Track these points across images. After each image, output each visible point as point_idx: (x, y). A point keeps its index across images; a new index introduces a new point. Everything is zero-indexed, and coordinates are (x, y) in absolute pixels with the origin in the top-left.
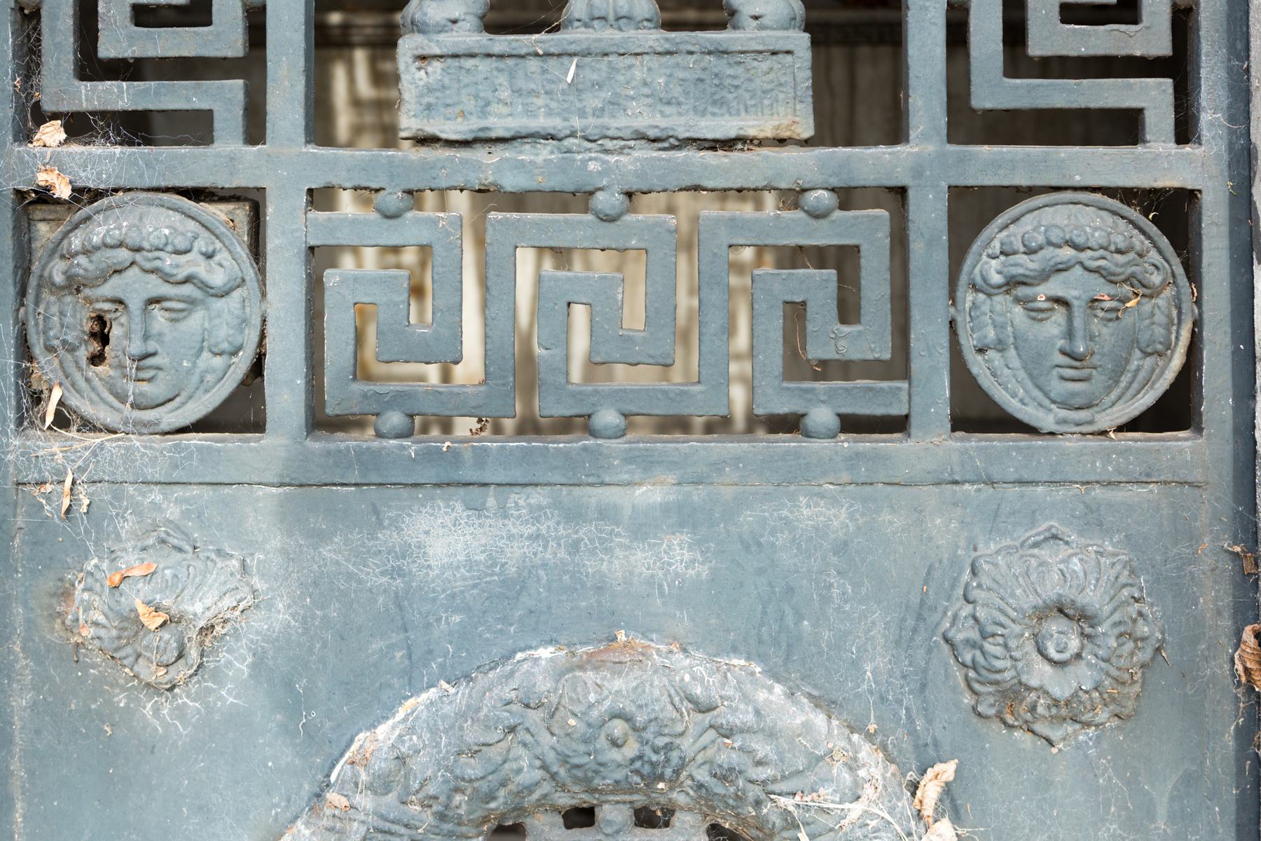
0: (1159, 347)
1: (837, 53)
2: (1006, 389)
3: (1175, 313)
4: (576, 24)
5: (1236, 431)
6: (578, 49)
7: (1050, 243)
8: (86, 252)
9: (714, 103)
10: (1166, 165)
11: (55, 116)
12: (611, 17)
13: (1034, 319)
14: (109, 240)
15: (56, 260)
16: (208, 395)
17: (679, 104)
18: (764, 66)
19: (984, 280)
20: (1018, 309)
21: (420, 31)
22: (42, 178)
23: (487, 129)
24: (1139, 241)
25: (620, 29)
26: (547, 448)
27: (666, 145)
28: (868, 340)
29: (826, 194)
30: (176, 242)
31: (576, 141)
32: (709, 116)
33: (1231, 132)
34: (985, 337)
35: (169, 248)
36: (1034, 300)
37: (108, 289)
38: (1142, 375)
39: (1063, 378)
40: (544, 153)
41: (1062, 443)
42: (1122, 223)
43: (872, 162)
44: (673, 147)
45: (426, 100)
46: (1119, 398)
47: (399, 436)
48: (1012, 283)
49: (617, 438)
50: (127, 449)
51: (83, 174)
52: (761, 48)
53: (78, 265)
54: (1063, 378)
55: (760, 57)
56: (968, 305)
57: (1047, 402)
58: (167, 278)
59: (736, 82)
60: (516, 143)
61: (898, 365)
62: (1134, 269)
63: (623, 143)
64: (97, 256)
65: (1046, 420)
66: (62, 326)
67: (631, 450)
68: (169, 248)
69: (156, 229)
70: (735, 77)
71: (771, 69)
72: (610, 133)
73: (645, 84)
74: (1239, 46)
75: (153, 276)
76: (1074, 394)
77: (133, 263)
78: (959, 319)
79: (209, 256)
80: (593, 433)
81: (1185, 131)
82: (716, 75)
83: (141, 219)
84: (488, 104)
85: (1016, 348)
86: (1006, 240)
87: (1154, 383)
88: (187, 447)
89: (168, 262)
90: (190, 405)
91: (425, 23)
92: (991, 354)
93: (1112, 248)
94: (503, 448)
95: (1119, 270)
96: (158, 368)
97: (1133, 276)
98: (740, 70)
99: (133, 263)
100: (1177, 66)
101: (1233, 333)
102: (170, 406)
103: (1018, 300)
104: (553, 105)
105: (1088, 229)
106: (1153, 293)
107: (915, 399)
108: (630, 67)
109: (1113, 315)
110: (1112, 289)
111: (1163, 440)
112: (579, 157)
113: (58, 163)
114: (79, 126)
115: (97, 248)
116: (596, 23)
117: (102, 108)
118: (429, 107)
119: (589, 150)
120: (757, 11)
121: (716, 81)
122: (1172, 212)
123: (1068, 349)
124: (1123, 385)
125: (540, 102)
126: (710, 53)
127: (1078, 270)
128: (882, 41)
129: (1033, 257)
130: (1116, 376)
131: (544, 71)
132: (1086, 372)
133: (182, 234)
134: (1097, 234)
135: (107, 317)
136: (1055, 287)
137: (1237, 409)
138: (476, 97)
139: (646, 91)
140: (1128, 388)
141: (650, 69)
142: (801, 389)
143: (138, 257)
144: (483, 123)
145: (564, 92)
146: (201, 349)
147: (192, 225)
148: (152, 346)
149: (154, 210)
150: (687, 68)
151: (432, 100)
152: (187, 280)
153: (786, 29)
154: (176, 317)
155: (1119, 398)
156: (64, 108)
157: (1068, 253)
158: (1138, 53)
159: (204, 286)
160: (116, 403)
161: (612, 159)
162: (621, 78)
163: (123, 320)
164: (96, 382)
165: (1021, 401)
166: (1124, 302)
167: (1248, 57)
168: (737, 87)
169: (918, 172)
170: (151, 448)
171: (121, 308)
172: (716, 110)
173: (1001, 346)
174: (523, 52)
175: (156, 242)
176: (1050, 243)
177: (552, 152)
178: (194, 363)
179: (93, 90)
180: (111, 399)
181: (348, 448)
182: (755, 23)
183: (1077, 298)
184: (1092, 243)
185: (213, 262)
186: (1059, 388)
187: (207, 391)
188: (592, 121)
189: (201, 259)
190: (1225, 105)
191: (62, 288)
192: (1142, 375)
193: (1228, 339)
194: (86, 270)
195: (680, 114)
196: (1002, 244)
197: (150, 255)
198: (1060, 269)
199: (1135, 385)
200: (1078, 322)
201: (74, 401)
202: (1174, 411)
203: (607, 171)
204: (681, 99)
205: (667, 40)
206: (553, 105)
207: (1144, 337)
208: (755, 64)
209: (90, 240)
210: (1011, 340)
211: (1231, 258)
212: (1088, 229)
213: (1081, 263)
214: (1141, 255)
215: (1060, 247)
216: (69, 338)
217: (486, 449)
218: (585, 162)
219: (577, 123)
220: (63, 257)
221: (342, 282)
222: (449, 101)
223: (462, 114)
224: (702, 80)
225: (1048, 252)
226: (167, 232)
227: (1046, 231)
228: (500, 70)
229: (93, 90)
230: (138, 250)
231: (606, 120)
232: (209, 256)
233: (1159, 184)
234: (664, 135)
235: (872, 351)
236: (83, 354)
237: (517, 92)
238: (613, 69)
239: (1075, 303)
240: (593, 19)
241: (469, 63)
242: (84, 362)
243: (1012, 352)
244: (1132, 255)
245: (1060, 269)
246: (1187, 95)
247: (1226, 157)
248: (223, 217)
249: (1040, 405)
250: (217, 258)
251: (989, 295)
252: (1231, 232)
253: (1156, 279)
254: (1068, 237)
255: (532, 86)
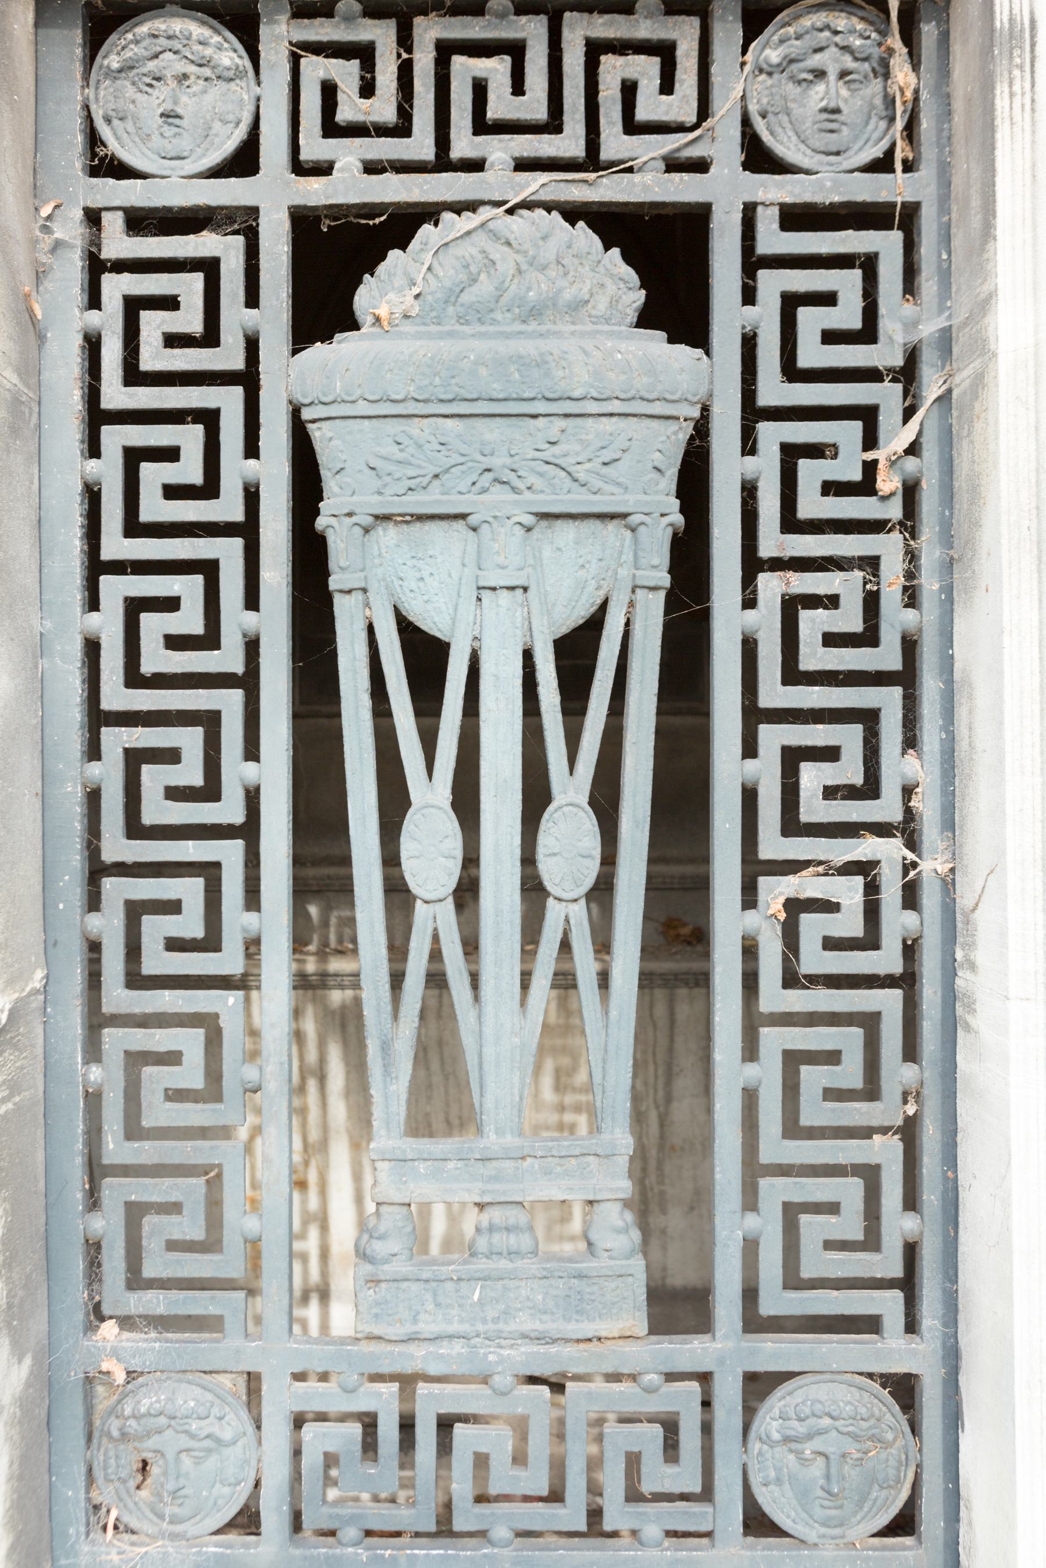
0: (892, 1483)
1: (660, 994)
2: (783, 1512)
3: (903, 1457)
4: (480, 1256)
5: (946, 1545)
6: (482, 1276)
7: (814, 1415)
8: (134, 1417)
9: (577, 1312)
10: (897, 1357)
11: (111, 1318)
12: (505, 1252)
13: (803, 1465)
14: (152, 1412)
15: (113, 1418)
16: (220, 1514)
17: (553, 1313)
18: (613, 1285)
19: (768, 1437)
20: (792, 1457)
21: (370, 1262)
22: (105, 1366)
23: (418, 1333)
24: (878, 1409)
25: (511, 1261)
26: (459, 1555)
27: (543, 1342)
28: (686, 1476)
29: (655, 1376)
30: (200, 1411)
31: (480, 1340)
32: (573, 1322)
33: (945, 1334)
34: (768, 1476)
35: (195, 1416)
36: (803, 1453)
37: (151, 1443)
38: (879, 1502)
39: (822, 1506)
40: (458, 1348)
41: (822, 1552)
42: (866, 1395)
43: (691, 1351)
44: (548, 1343)
45: (375, 1311)
46: (863, 1518)
47: (354, 1545)
48: (787, 1440)
49: (507, 1546)
50: (164, 1553)
51: (133, 1362)
52: (610, 1273)
53: (130, 1426)
54: (822, 1506)
55: (610, 1279)
56: (756, 1452)
57: (811, 1522)
58: (192, 1436)
59: (593, 1297)
60: (438, 1341)
61: (707, 1494)
62: (873, 1431)
63: (513, 1342)
64: (143, 1421)
65: (811, 1536)
66: (118, 1467)
67: (517, 1556)
68: (195, 1416)
69: (185, 1402)
70: (591, 1294)
71: (618, 1287)
72: (504, 1335)
73: (528, 1299)
74: (951, 1272)
75: (183, 1435)
76: (830, 1518)
77: (169, 1426)
78: (750, 1464)
79: (221, 1419)
80: (492, 1544)
81: (911, 1326)
82: (579, 1293)
83: (173, 1393)
84: (418, 1313)
85: (790, 1484)
86: (783, 1409)
87: (888, 1508)
88: (206, 1553)
89: (194, 1426)
90: (207, 1521)
91: (373, 1258)
92: (772, 1487)
93: (859, 1417)
94: (427, 1555)
95: (863, 1433)
96: (186, 1497)
97: (873, 1435)
98: (595, 1288)
99: (169, 1426)
100: (908, 1283)
101: (945, 1476)
102: (192, 1521)
103: (791, 1451)
104: (464, 1314)
105: (841, 1404)
106: (887, 1445)
107: (718, 1521)
108: (518, 1287)
109: (859, 1463)
110: (858, 1446)
111: (892, 1548)
112: (482, 1351)
113: (116, 1354)
114: (126, 1322)
115: (143, 1416)
116: (494, 1256)
117: (145, 1313)
118: (376, 1316)
119: (490, 1346)
120: (608, 1246)
121: (579, 1297)
122: (903, 1389)
123: (826, 1488)
124: (866, 1509)
125: (454, 1312)
126: (574, 1277)
127: (834, 1434)
128: (697, 985)
129: (802, 1423)
130: (860, 1504)
131: (457, 1291)
132: (840, 1502)
133: (203, 1404)
134: (847, 1408)
135: (150, 1461)
136: (817, 1444)
137: (946, 1529)
138: (410, 1308)
139: (529, 1304)
140: (869, 1512)
141: (532, 1289)
142: (636, 1512)
143: (173, 1422)
144: (414, 1328)
145: (471, 1305)
146: (215, 1483)
147: (209, 1396)
148: (182, 1482)
149: (184, 1385)
150: (558, 1288)
151: (378, 1311)
152: (207, 1437)
153: (628, 1259)
154: (198, 1461)
155: (863, 1518)
156: (118, 1313)
157: (827, 1421)
158: (879, 1276)
159: (218, 1441)
160: (155, 1519)
161: (506, 1352)
162: (512, 1295)
163: (161, 1462)
164: (142, 1505)
165: (793, 1521)
166: (866, 1453)
167: (957, 1282)
168: (593, 1301)
169: (721, 1362)
170: (180, 1553)
171: (159, 1455)
172: (578, 1318)
173: (779, 1481)
174: (443, 1278)
175: (186, 1412)
176: (814, 1415)
177: (463, 1347)
178: (210, 1493)
179: (140, 1299)
180: (151, 1516)
181: (319, 1554)
182: (606, 1254)
183: (833, 1454)
184: (844, 1415)
185: (223, 1422)
186: (819, 1513)
187: (218, 1511)
188: (491, 1326)
189: (216, 1421)
190: (940, 1315)
191: (118, 1440)
192: (879, 1502)
193: (941, 1480)
194: (136, 1431)
195: (553, 1321)
196: (781, 1412)
197: (181, 1422)
198: (820, 1433)
199: (875, 1509)
200: (833, 1471)
201: (126, 1519)
202: (903, 1524)
203: (501, 1361)
204: (554, 1310)
205: (544, 1269)
206: (464, 1314)
207: (881, 1477)
208: (606, 1284)
209: (139, 1411)
210: (787, 1478)
211: (944, 1423)
212: (841, 1404)
213: (837, 1429)
214: (878, 1420)
215: (821, 1417)
216: (122, 1475)
217: (415, 1555)
218: (486, 1355)
219: (480, 1327)
220: (117, 1417)
221: (314, 1437)
222: (390, 1312)
223: (400, 1321)
224: (568, 1296)
225: (812, 1421)
226: (192, 1404)
227: (812, 1405)
228: (427, 1290)
229: (140, 1299)
230: (174, 1418)
231: (501, 1326)
232: (221, 1419)
233: (893, 1371)
234: (542, 1336)
235: (687, 1486)
236: (132, 1484)
237: (438, 1305)
238: (505, 1288)
239: (832, 1457)
240: (492, 1254)
241: (405, 1285)
242: (133, 1489)
243: (787, 1486)
244: (872, 1421)
245: (820, 1433)
246: (914, 1306)
247: (940, 1352)
248: (229, 1385)
249: (807, 1524)
250: (227, 1418)
251: (771, 1447)
252: (944, 1404)
253: (889, 1436)
254: (827, 1410)
255: (449, 1301)
